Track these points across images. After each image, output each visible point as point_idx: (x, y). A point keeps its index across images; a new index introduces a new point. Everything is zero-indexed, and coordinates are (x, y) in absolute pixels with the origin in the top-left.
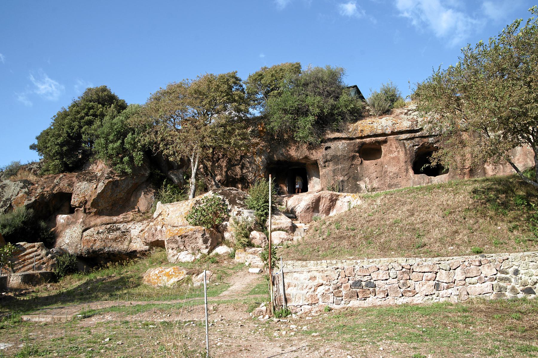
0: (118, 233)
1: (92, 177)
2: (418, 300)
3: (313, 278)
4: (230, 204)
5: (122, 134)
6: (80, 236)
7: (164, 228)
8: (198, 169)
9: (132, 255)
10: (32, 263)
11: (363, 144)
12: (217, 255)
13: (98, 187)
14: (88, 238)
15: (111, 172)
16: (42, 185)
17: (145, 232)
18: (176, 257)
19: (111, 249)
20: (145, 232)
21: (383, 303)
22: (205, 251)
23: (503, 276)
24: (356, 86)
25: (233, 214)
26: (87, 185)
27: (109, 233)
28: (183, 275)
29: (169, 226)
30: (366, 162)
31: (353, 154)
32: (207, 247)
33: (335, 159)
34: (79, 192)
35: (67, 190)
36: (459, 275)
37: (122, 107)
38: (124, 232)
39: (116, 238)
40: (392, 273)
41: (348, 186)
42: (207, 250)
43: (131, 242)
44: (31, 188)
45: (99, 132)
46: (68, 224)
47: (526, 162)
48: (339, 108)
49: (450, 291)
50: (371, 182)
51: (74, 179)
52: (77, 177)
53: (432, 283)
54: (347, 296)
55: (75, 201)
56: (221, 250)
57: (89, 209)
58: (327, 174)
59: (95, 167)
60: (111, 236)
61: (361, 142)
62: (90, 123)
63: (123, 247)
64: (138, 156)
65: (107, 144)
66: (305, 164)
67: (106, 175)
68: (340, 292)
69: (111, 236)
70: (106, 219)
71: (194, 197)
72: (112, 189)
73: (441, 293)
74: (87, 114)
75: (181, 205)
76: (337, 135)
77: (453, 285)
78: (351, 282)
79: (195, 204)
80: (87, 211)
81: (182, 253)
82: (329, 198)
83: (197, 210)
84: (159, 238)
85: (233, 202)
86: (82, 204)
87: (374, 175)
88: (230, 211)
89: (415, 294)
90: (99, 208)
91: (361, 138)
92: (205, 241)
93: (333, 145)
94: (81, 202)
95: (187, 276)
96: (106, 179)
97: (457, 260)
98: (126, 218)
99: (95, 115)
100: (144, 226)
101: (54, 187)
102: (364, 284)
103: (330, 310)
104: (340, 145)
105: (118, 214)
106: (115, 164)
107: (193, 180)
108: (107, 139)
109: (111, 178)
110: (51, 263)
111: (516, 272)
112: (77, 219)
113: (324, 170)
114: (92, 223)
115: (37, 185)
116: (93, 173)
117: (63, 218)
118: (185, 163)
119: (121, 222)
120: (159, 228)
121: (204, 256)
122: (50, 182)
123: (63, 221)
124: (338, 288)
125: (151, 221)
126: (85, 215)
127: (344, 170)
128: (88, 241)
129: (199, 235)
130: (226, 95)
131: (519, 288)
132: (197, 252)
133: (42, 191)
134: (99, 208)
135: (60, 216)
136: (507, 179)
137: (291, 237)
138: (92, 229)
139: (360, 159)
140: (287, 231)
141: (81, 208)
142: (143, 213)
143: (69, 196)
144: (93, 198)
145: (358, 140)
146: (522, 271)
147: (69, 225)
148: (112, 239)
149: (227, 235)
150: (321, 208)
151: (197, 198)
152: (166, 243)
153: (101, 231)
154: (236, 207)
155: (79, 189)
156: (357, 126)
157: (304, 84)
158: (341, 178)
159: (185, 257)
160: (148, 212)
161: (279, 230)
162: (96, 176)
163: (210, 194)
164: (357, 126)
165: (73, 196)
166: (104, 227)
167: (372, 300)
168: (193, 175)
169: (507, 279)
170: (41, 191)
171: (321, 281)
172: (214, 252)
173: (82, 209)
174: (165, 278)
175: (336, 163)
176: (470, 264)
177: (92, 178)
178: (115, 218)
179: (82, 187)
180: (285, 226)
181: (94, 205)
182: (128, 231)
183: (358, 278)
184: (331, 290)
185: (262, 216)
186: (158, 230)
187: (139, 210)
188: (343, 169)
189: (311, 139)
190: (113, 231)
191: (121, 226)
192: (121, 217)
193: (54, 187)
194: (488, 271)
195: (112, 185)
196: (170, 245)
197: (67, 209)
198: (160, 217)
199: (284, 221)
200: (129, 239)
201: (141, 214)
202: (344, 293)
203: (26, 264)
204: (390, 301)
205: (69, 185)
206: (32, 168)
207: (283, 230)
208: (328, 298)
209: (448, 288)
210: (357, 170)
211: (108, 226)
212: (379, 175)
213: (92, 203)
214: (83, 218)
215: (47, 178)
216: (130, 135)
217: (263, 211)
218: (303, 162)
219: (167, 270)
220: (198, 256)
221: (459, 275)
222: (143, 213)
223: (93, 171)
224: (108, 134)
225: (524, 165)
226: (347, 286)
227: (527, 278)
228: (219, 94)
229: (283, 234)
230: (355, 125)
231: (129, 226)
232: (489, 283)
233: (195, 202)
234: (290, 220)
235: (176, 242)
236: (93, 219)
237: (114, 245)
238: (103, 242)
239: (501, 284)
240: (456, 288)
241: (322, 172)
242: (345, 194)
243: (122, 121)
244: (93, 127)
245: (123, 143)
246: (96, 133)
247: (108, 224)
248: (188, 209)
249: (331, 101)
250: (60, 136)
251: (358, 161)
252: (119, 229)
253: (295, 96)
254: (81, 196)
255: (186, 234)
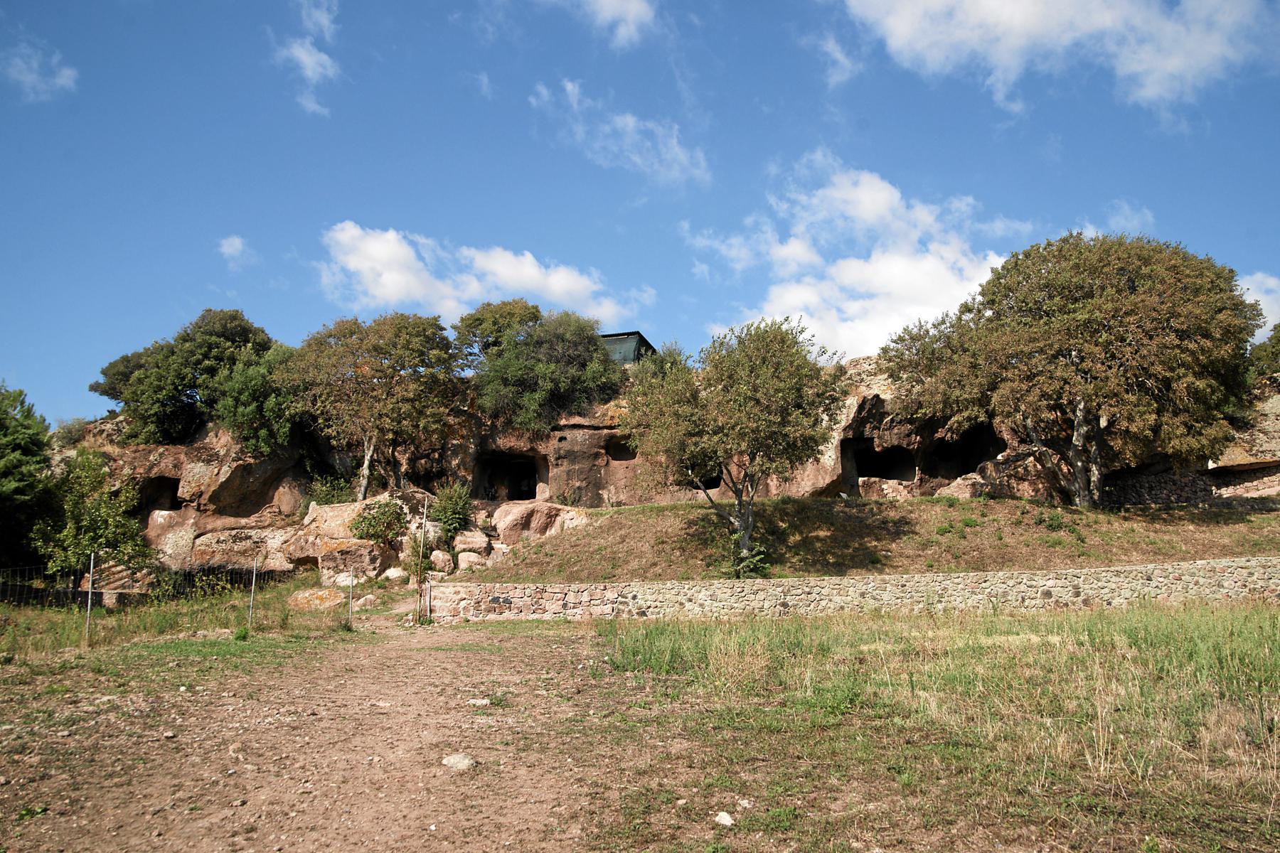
0: (248, 543)
1: (211, 456)
2: (547, 616)
3: (457, 593)
4: (410, 513)
5: (260, 395)
6: (191, 544)
7: (318, 540)
8: (372, 456)
9: (267, 577)
10: (121, 579)
11: (612, 437)
12: (387, 579)
13: (221, 472)
14: (203, 548)
15: (242, 451)
16: (131, 463)
17: (290, 545)
18: (332, 579)
19: (237, 566)
20: (290, 545)
21: (516, 618)
22: (372, 574)
23: (623, 600)
24: (638, 333)
25: (413, 526)
26: (204, 468)
27: (234, 542)
28: (341, 598)
29: (326, 538)
30: (615, 463)
31: (596, 450)
32: (374, 569)
33: (570, 456)
34: (191, 479)
35: (170, 473)
36: (585, 597)
37: (263, 346)
38: (258, 542)
39: (245, 551)
40: (527, 591)
41: (587, 495)
42: (375, 572)
43: (266, 557)
44: (114, 467)
45: (226, 387)
46: (169, 526)
47: (817, 480)
48: (584, 382)
49: (575, 610)
50: (617, 492)
51: (182, 457)
52: (186, 454)
53: (561, 602)
54: (485, 610)
55: (184, 491)
56: (393, 573)
57: (205, 505)
58: (559, 477)
59: (215, 440)
60: (238, 547)
61: (609, 434)
62: (212, 371)
63: (255, 564)
64: (283, 429)
65: (236, 407)
66: (534, 457)
67: (234, 455)
68: (480, 606)
69: (238, 547)
70: (230, 521)
71: (365, 498)
72: (242, 476)
73: (568, 612)
74: (206, 356)
75: (344, 509)
76: (577, 420)
77: (579, 605)
78: (490, 598)
79: (364, 509)
80: (202, 508)
81: (342, 575)
82: (546, 512)
83: (365, 518)
84: (311, 553)
85: (414, 511)
86: (194, 497)
87: (623, 482)
88: (409, 522)
89: (545, 611)
90: (221, 504)
91: (611, 428)
92: (373, 560)
93: (568, 434)
94: (193, 495)
95: (344, 600)
96: (233, 460)
97: (584, 586)
98: (261, 521)
99: (219, 359)
100: (288, 534)
101: (151, 468)
102: (501, 600)
103: (468, 621)
104: (580, 435)
105: (248, 516)
106: (246, 439)
107: (365, 471)
108: (237, 400)
109: (240, 459)
110: (147, 581)
111: (634, 597)
112: (185, 519)
113: (555, 470)
114: (209, 527)
115: (121, 462)
116: (211, 449)
117: (162, 516)
118: (354, 445)
119: (252, 528)
120: (311, 539)
121: (370, 580)
122: (142, 459)
123: (163, 521)
124: (478, 603)
125: (300, 529)
126: (198, 513)
127: (582, 473)
128: (204, 553)
129: (365, 552)
130: (419, 356)
131: (635, 611)
132: (361, 574)
133: (133, 473)
134: (221, 504)
135: (157, 512)
136: (781, 506)
137: (483, 561)
138: (209, 535)
139: (605, 458)
140: (479, 553)
141: (193, 502)
142: (286, 516)
143: (175, 483)
144: (213, 489)
145: (606, 431)
146: (639, 597)
147: (172, 527)
148: (239, 552)
149: (402, 556)
150: (533, 525)
151: (368, 501)
152: (320, 560)
153: (222, 538)
154: (417, 517)
155: (191, 474)
156: (607, 409)
157: (537, 342)
158: (578, 484)
159: (345, 579)
160: (294, 514)
161: (470, 551)
162: (217, 454)
163: (384, 497)
164: (607, 409)
165: (181, 484)
166: (227, 533)
167: (507, 615)
168: (366, 463)
169: (626, 603)
170: (130, 472)
171: (464, 596)
172: (383, 576)
173: (195, 504)
174: (318, 602)
175: (573, 462)
176: (596, 588)
177: (211, 458)
178: (243, 521)
179: (195, 471)
180: (478, 546)
181: (212, 499)
182: (263, 541)
183: (497, 595)
184: (472, 604)
185: (449, 531)
186: (310, 541)
187: (280, 511)
188: (581, 471)
189: (534, 426)
190: (241, 539)
191: (252, 533)
192: (252, 520)
193: (151, 468)
194: (610, 595)
195: (243, 472)
196: (325, 563)
197: (167, 502)
198: (314, 525)
199: (478, 539)
200: (264, 553)
201: (283, 517)
202: (483, 607)
203: (112, 580)
204: (523, 616)
205: (175, 466)
206: (104, 430)
207: (474, 552)
208: (469, 611)
209: (574, 608)
210: (600, 474)
211: (234, 532)
212: (628, 484)
213: (211, 496)
214: (194, 518)
215: (135, 452)
216: (272, 400)
217: (452, 524)
218: (530, 454)
219: (320, 593)
220: (362, 580)
221: (585, 597)
222: (286, 516)
223: (211, 446)
224: (240, 393)
225: (813, 484)
226: (486, 602)
227: (643, 602)
228: (407, 353)
229: (474, 557)
230: (606, 407)
231: (265, 534)
232: (610, 606)
233: (363, 506)
234: (487, 539)
235: (334, 559)
236: (209, 520)
237: (242, 560)
238: (226, 556)
239: (620, 607)
240: (581, 608)
241: (553, 472)
242: (569, 508)
243: (264, 377)
244: (217, 378)
245: (260, 409)
246: (222, 388)
247: (234, 529)
248: (354, 515)
249: (573, 371)
250: (160, 389)
251: (601, 462)
252: (250, 537)
253: (521, 360)
254: (193, 485)
255: (348, 550)
